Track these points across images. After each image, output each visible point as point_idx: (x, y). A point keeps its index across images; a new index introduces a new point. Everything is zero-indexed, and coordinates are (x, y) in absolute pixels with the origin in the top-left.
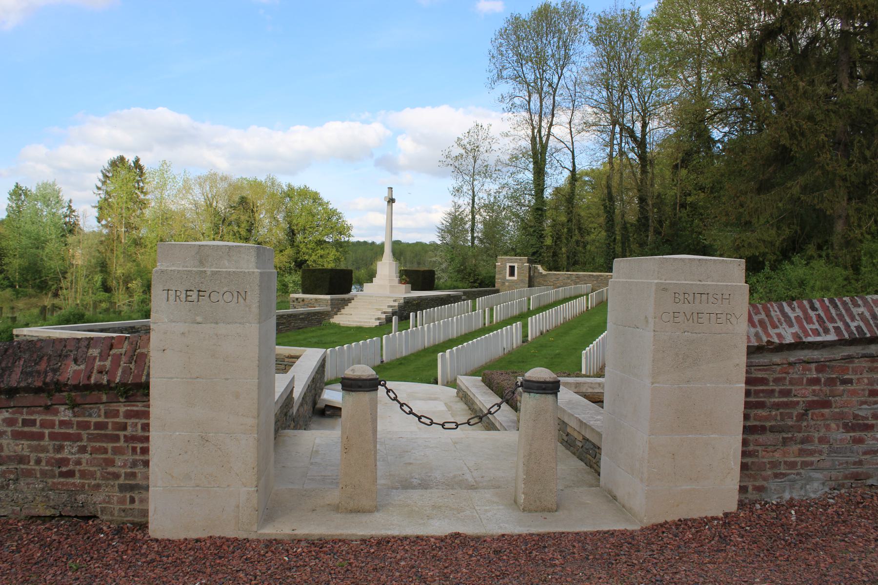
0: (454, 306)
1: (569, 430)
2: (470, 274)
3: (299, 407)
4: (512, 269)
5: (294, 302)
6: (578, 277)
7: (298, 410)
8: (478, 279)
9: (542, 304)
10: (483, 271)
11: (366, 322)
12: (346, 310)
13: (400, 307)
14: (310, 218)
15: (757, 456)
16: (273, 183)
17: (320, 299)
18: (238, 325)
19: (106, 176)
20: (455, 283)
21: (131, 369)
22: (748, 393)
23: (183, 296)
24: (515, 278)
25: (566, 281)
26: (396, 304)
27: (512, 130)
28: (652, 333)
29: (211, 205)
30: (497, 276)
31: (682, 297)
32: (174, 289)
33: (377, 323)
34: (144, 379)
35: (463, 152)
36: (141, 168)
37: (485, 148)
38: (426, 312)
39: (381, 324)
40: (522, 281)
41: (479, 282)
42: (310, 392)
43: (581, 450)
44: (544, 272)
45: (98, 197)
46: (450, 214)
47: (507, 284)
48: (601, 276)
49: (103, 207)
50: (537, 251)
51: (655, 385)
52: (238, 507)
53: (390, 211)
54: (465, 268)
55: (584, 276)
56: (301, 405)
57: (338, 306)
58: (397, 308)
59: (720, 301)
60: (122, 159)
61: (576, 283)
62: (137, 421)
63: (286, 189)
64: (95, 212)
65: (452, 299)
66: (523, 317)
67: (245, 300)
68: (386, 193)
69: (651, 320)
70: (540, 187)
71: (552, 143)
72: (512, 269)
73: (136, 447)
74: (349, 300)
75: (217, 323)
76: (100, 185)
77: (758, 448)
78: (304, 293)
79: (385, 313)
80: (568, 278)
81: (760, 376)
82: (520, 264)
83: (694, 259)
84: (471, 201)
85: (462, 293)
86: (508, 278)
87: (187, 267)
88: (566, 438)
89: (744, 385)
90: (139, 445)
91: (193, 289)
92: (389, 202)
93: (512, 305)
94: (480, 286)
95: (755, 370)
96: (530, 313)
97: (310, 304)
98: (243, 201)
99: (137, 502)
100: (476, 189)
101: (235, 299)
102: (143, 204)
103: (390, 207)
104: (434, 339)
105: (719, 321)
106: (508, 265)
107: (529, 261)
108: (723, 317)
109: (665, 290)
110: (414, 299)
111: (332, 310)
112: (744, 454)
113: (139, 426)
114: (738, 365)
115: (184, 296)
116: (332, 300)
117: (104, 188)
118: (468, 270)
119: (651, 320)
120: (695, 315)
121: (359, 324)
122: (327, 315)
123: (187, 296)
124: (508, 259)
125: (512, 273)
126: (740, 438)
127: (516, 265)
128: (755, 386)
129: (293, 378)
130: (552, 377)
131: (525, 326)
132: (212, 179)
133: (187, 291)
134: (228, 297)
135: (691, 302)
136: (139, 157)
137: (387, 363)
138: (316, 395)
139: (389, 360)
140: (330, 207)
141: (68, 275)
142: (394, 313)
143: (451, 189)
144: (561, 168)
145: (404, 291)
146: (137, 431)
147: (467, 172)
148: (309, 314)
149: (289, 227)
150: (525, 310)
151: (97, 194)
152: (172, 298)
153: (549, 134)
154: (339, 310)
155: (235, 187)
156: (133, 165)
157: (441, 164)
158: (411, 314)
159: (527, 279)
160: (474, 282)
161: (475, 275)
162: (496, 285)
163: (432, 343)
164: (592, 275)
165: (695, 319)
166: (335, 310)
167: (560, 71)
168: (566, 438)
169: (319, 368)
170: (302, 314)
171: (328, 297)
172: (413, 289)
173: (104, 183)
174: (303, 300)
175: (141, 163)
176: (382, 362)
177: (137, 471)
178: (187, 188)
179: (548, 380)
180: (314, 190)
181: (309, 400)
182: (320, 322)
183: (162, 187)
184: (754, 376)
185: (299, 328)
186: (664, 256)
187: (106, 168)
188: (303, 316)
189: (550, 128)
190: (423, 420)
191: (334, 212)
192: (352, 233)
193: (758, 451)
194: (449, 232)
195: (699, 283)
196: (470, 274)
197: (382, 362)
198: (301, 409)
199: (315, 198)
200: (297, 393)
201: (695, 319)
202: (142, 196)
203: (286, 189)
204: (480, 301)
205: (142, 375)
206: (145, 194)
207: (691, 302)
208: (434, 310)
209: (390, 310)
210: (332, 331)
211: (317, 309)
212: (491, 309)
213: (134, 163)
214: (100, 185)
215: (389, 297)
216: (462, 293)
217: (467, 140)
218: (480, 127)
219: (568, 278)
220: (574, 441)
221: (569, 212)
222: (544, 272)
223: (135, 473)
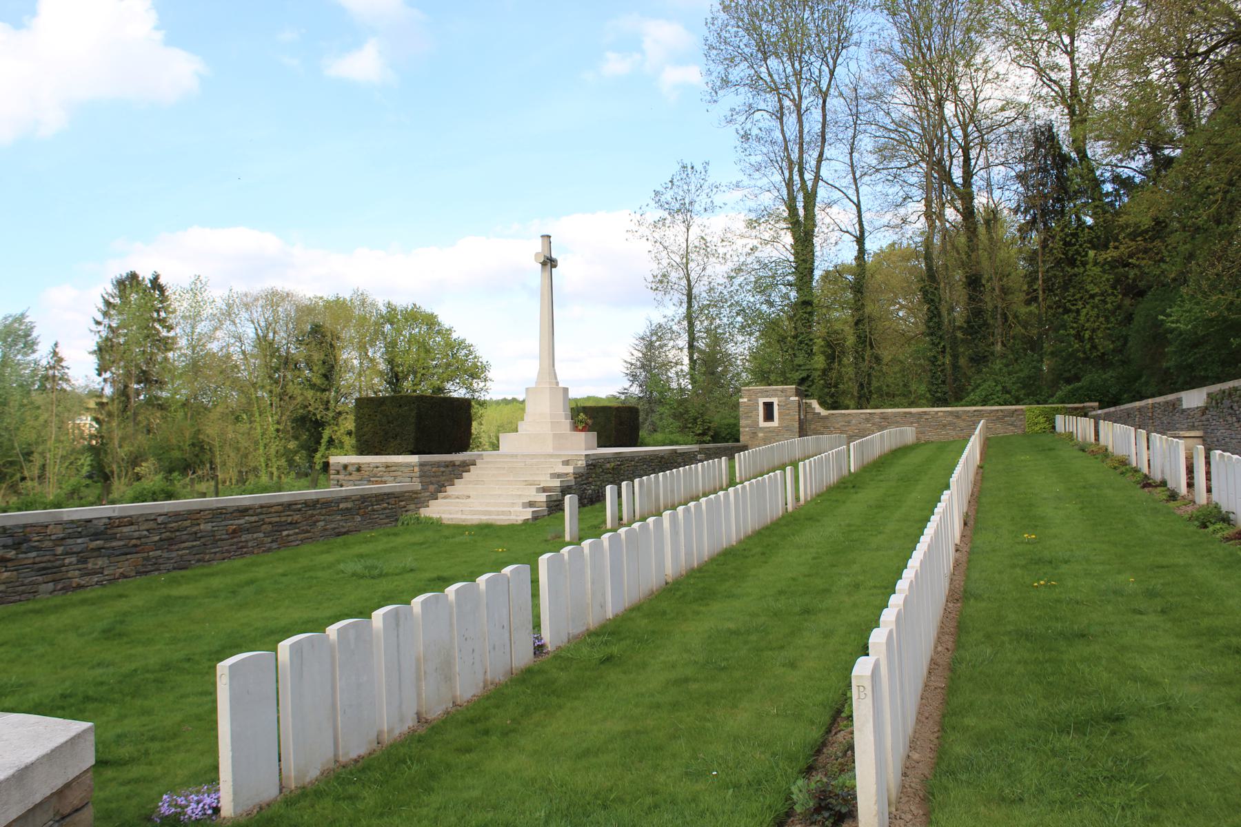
0: (696, 469)
2: (695, 419)
4: (769, 407)
5: (338, 473)
6: (884, 417)
8: (709, 429)
10: (718, 418)
11: (503, 513)
12: (459, 488)
13: (578, 476)
14: (423, 355)
16: (363, 302)
19: (108, 303)
20: (672, 437)
24: (775, 423)
25: (863, 426)
26: (570, 469)
27: (745, 178)
29: (265, 337)
30: (743, 422)
33: (527, 514)
35: (665, 214)
36: (161, 289)
37: (703, 206)
38: (641, 484)
39: (536, 517)
40: (788, 429)
41: (711, 433)
45: (98, 336)
46: (643, 339)
47: (761, 435)
48: (925, 413)
49: (106, 352)
50: (808, 376)
53: (547, 281)
54: (687, 412)
55: (896, 415)
57: (439, 481)
58: (572, 478)
60: (133, 277)
61: (882, 428)
63: (384, 311)
64: (93, 361)
65: (680, 460)
68: (537, 246)
70: (808, 266)
71: (822, 193)
72: (769, 407)
73: (772, 404)
74: (466, 466)
76: (100, 318)
78: (361, 452)
79: (544, 490)
80: (867, 420)
82: (783, 397)
84: (685, 298)
86: (762, 424)
92: (544, 264)
93: (827, 458)
94: (715, 439)
97: (373, 475)
98: (316, 330)
100: (693, 276)
102: (167, 344)
103: (547, 274)
104: (689, 554)
106: (761, 401)
107: (798, 393)
110: (607, 459)
111: (425, 489)
116: (422, 465)
117: (106, 321)
118: (693, 413)
121: (485, 519)
122: (414, 499)
124: (762, 391)
125: (769, 416)
127: (775, 400)
132: (274, 299)
136: (159, 272)
137: (557, 656)
139: (562, 640)
140: (454, 336)
141: (36, 457)
142: (565, 490)
143: (650, 279)
144: (838, 234)
145: (583, 445)
147: (675, 249)
148: (364, 499)
149: (391, 370)
151: (95, 332)
153: (818, 177)
154: (441, 488)
155: (306, 310)
156: (149, 285)
157: (629, 235)
158: (608, 488)
159: (796, 425)
160: (704, 434)
161: (704, 421)
162: (742, 438)
163: (683, 567)
164: (910, 413)
166: (432, 488)
167: (831, 62)
170: (346, 499)
171: (414, 459)
173: (105, 314)
174: (359, 469)
175: (162, 281)
176: (539, 649)
178: (229, 313)
180: (429, 310)
182: (394, 518)
183: (194, 318)
185: (339, 535)
187: (110, 291)
188: (349, 505)
189: (818, 167)
191: (461, 344)
192: (489, 375)
194: (643, 367)
196: (695, 419)
197: (539, 649)
199: (430, 321)
202: (164, 333)
203: (384, 311)
206: (170, 328)
208: (657, 479)
209: (556, 483)
210: (418, 538)
211: (390, 486)
213: (151, 282)
214: (100, 318)
215: (551, 456)
217: (671, 193)
218: (689, 170)
219: (867, 420)
221: (858, 306)
222: (824, 412)
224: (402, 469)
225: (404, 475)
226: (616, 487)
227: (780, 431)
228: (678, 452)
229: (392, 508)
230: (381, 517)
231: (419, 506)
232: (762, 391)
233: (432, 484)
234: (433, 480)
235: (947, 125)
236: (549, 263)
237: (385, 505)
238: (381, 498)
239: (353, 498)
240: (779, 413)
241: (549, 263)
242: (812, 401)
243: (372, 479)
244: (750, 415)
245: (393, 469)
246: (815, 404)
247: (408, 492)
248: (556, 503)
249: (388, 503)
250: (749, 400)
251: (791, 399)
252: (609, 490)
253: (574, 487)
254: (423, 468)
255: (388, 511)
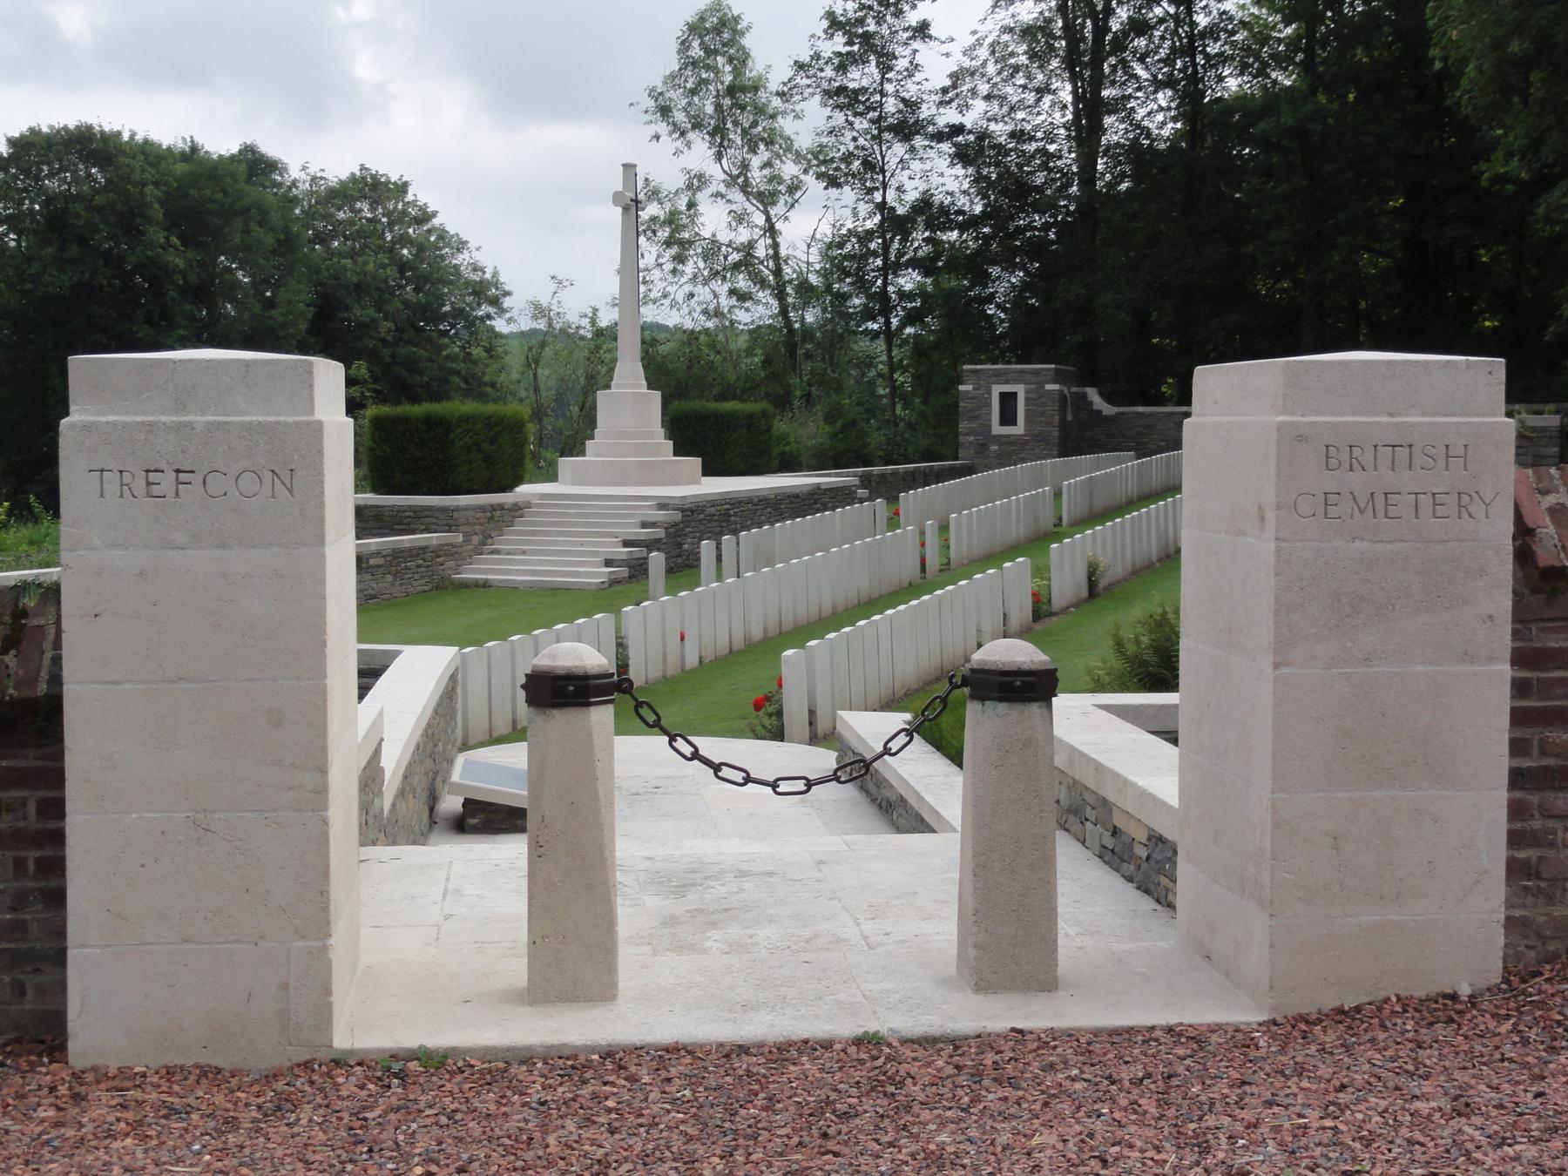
1: (1118, 820)
3: (396, 797)
4: (1008, 400)
7: (394, 805)
9: (1099, 504)
15: (1552, 844)
17: (430, 509)
18: (276, 550)
21: (7, 667)
22: (1520, 688)
23: (139, 485)
24: (1019, 429)
28: (1272, 546)
31: (1345, 457)
32: (115, 466)
34: (42, 688)
42: (422, 762)
43: (1145, 865)
44: (1107, 409)
51: (1285, 670)
52: (285, 987)
56: (401, 793)
59: (1441, 463)
62: (26, 793)
66: (1037, 541)
67: (290, 490)
69: (1271, 516)
72: (1008, 400)
73: (25, 860)
75: (223, 546)
77: (1551, 823)
81: (1554, 645)
83: (1417, 362)
85: (855, 481)
86: (997, 429)
87: (144, 413)
88: (1109, 841)
89: (1508, 667)
90: (33, 855)
91: (161, 466)
95: (1542, 630)
96: (1055, 532)
99: (30, 996)
101: (267, 490)
105: (1441, 510)
108: (1452, 501)
109: (1302, 438)
112: (1515, 839)
113: (32, 808)
114: (1491, 617)
115: (143, 482)
119: (1271, 516)
120: (1380, 499)
123: (149, 484)
124: (997, 374)
125: (1008, 418)
126: (1502, 796)
127: (1020, 390)
128: (1541, 670)
129: (381, 714)
130: (1036, 659)
131: (1041, 572)
133: (148, 471)
134: (248, 483)
135: (1370, 465)
138: (436, 773)
146: (25, 818)
150: (1047, 521)
152: (112, 488)
165: (1380, 507)
166: (475, 539)
168: (1109, 841)
169: (441, 698)
170: (377, 554)
172: (708, 471)
177: (28, 917)
179: (1025, 667)
181: (420, 783)
184: (1539, 645)
186: (272, 419)
188: (380, 561)
190: (725, 772)
193: (1554, 833)
195: (1386, 419)
198: (402, 807)
200: (393, 761)
201: (1380, 507)
204: (911, 499)
205: (36, 679)
207: (1370, 465)
212: (944, 527)
216: (855, 481)
220: (1131, 847)
222: (1107, 409)
223: (25, 922)
224: (437, 514)
225: (440, 522)
226: (714, 543)
227: (1027, 442)
228: (823, 487)
229: (428, 566)
230: (416, 576)
231: (459, 563)
232: (997, 374)
233: (476, 534)
234: (477, 528)
235: (407, 806)
236: (682, 638)
237: (421, 562)
238: (415, 552)
239: (384, 553)
240: (1027, 411)
241: (682, 638)
242: (1089, 390)
243: (396, 527)
244: (977, 413)
245: (426, 513)
246: (1093, 395)
247: (447, 545)
248: (640, 562)
249: (424, 560)
250: (975, 389)
251: (1049, 387)
252: (707, 547)
253: (665, 541)
254: (1533, 734)
255: (423, 569)
